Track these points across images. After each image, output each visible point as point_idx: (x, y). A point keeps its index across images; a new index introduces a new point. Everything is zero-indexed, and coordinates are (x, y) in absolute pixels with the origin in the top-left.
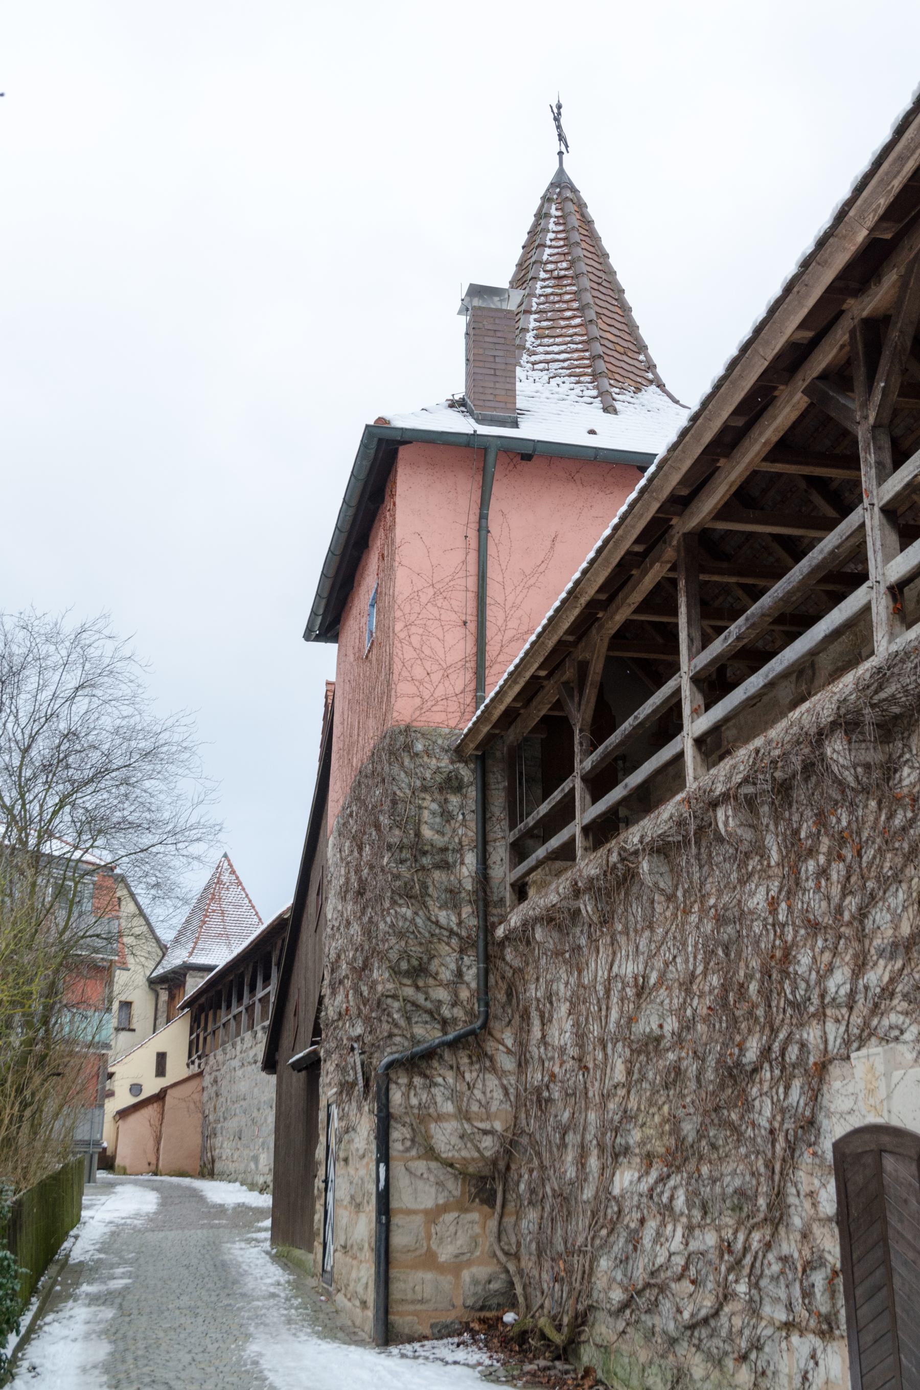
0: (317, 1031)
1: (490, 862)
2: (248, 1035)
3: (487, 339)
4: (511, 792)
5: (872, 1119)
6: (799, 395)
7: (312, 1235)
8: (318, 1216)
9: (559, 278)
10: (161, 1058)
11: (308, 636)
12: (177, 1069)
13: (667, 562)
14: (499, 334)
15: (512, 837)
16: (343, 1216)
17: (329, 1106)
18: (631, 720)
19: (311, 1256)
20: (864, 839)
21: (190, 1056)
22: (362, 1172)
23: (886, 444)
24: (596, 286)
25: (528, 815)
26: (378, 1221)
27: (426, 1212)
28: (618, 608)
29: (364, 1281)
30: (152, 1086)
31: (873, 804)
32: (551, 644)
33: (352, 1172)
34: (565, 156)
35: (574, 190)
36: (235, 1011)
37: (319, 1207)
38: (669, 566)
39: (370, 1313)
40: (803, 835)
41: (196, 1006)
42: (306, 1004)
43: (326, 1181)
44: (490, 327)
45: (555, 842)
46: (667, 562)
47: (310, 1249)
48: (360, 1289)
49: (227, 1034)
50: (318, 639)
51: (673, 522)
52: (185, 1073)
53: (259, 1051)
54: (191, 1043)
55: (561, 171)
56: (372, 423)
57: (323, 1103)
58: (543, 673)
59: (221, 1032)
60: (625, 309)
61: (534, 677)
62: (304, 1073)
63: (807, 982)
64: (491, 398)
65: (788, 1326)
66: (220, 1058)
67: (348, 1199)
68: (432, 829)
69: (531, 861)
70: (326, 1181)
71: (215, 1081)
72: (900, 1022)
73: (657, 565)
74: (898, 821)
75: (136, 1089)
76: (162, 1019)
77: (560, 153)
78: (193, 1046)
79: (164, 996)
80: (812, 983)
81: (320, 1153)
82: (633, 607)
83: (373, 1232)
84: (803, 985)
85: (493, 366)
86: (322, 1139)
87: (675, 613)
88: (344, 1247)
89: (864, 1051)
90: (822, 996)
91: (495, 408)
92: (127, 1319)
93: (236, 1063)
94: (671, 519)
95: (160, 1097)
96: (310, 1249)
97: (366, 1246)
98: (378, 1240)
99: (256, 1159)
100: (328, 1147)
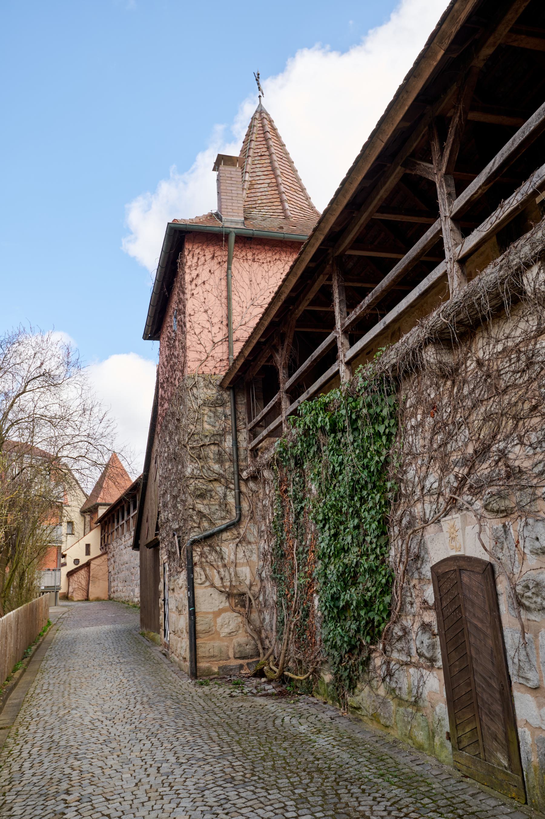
0: (157, 529)
1: (239, 439)
3: (228, 182)
5: (453, 553)
6: (399, 167)
7: (159, 626)
8: (162, 617)
9: (261, 156)
10: (88, 546)
12: (95, 551)
13: (327, 274)
14: (233, 179)
15: (249, 426)
16: (173, 616)
17: (164, 564)
18: (310, 357)
19: (159, 636)
20: (444, 403)
21: (101, 545)
22: (181, 595)
23: (452, 183)
27: (214, 613)
28: (301, 303)
29: (184, 648)
30: (84, 560)
31: (449, 383)
32: (266, 323)
33: (177, 595)
34: (262, 98)
35: (267, 114)
36: (121, 523)
38: (327, 276)
39: (188, 664)
40: (408, 406)
41: (103, 522)
42: (152, 516)
43: (164, 600)
44: (229, 176)
45: (272, 426)
46: (327, 274)
48: (183, 654)
49: (118, 534)
50: (150, 338)
51: (329, 251)
52: (100, 553)
54: (101, 539)
55: (260, 105)
56: (171, 222)
57: (161, 562)
59: (115, 533)
60: (295, 171)
61: (258, 343)
62: (152, 549)
63: (413, 483)
64: (231, 210)
66: (115, 545)
67: (175, 608)
68: (209, 424)
69: (260, 437)
70: (164, 600)
71: (113, 556)
72: (470, 499)
73: (321, 277)
74: (466, 391)
75: (76, 561)
76: (88, 529)
78: (103, 539)
79: (88, 518)
80: (416, 483)
81: (161, 587)
82: (308, 302)
83: (188, 624)
84: (411, 485)
85: (230, 195)
86: (162, 580)
87: (330, 301)
88: (174, 632)
89: (448, 518)
92: (67, 673)
93: (122, 547)
94: (328, 250)
95: (88, 565)
96: (159, 633)
97: (185, 631)
99: (133, 591)
100: (165, 583)
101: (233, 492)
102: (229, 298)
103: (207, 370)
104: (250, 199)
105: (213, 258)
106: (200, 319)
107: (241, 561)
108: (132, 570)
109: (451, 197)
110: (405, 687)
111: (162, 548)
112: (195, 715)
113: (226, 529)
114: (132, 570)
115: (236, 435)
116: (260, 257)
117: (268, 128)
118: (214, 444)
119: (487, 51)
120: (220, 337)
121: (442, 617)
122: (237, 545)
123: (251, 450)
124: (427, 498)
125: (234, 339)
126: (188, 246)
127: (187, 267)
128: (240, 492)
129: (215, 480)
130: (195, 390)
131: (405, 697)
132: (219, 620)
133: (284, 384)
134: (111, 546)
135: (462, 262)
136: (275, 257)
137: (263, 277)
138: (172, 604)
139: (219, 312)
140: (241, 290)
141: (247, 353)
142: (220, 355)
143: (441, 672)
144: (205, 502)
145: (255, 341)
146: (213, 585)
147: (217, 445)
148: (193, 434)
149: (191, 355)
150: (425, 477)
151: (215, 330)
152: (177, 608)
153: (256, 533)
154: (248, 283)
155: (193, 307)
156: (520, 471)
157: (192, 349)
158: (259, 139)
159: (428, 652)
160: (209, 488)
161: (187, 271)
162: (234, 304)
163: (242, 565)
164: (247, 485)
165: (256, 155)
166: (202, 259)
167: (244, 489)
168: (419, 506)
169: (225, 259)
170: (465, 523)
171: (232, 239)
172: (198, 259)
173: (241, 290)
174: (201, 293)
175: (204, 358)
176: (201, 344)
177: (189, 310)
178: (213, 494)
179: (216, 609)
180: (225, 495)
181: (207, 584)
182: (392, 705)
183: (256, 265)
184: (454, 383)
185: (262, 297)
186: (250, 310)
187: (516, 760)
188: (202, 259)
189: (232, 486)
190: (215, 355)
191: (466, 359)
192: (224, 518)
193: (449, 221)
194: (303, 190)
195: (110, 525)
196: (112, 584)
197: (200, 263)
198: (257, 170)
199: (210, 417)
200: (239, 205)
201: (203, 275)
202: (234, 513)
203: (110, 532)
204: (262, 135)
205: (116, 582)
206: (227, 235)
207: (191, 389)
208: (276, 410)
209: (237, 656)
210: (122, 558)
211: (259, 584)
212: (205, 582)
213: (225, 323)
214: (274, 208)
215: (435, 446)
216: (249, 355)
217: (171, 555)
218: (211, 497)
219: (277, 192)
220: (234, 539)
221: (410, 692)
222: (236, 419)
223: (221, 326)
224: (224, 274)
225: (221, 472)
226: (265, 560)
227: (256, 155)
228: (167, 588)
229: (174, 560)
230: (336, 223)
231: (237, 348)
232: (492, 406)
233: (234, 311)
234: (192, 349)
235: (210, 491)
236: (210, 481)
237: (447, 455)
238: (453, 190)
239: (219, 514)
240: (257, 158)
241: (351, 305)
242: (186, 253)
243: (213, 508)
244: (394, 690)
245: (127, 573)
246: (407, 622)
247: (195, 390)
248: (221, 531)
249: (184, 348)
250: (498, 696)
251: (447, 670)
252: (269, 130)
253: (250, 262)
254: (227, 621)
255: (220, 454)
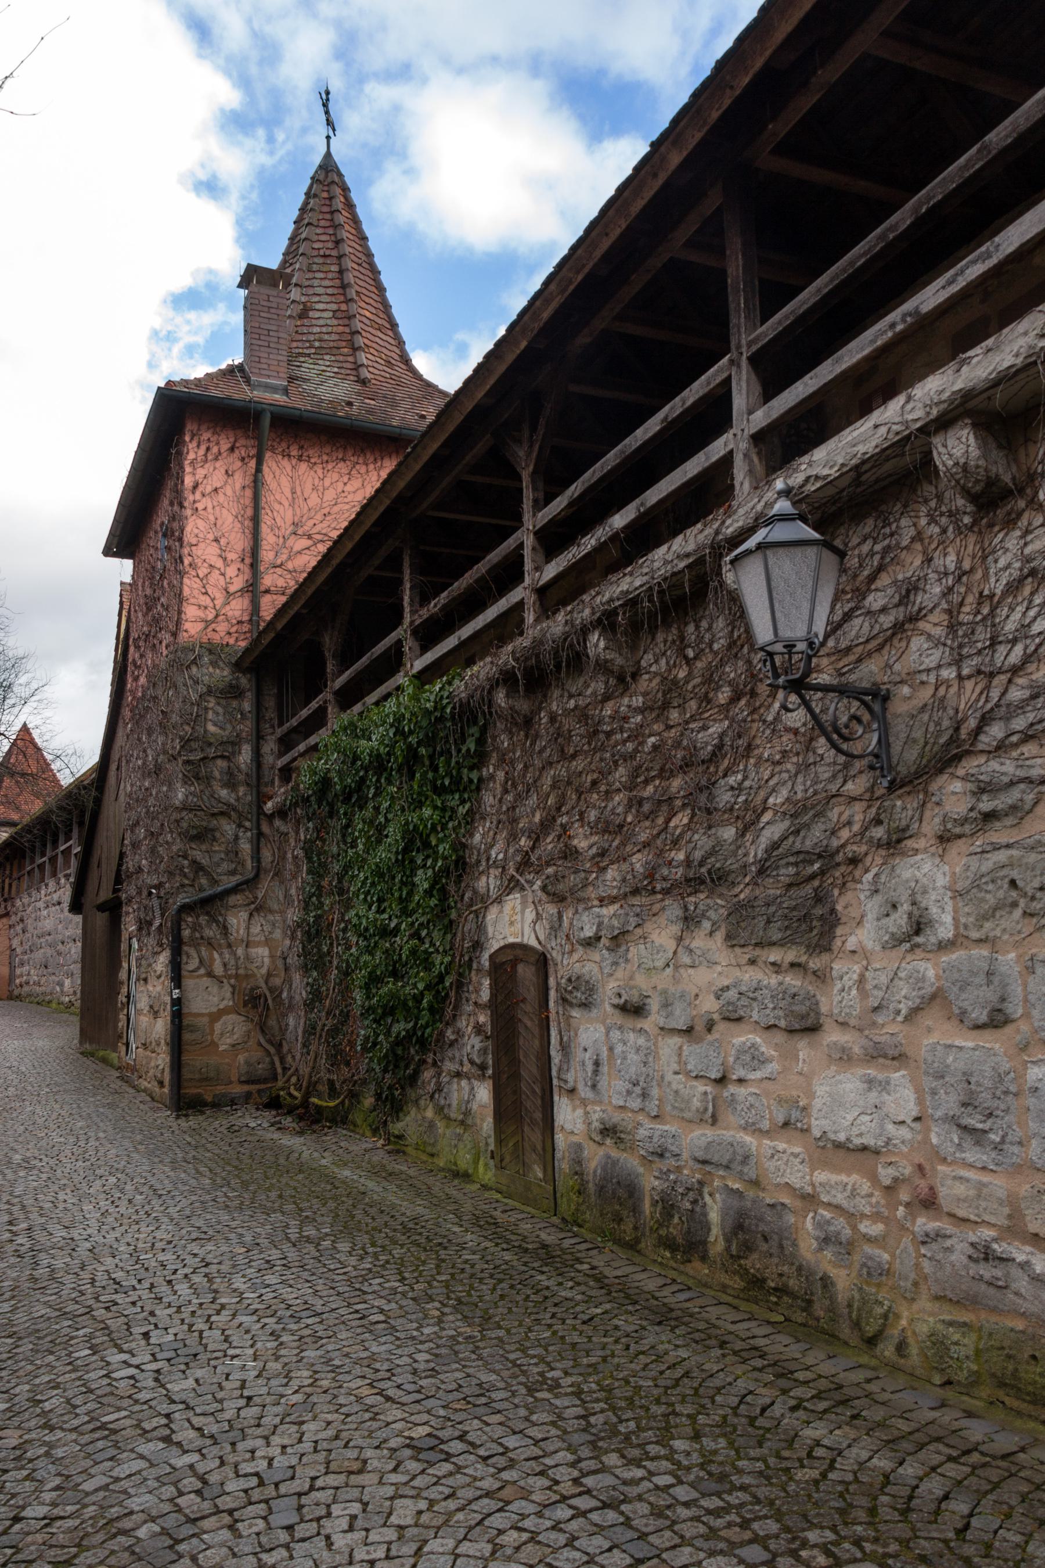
0: (118, 880)
2: (52, 883)
4: (279, 696)
9: (325, 256)
11: (107, 552)
15: (279, 732)
22: (159, 988)
24: (356, 267)
25: (294, 715)
26: (172, 1022)
27: (210, 1015)
33: (151, 988)
34: (332, 141)
35: (340, 175)
37: (122, 1017)
47: (115, 1049)
53: (65, 894)
55: (328, 155)
56: (162, 385)
57: (125, 936)
58: (304, 611)
60: (381, 289)
61: (297, 615)
62: (107, 913)
65: (458, 1075)
68: (215, 725)
69: (294, 753)
70: (128, 997)
71: (22, 920)
77: (328, 138)
81: (123, 975)
86: (125, 965)
88: (144, 1045)
90: (488, 859)
91: (269, 376)
98: (172, 1038)
101: (249, 834)
102: (256, 520)
103: (216, 638)
104: (300, 337)
105: (232, 449)
106: (206, 553)
107: (257, 939)
108: (60, 947)
109: (539, 505)
110: (455, 1103)
111: (127, 913)
112: (178, 1151)
113: (234, 890)
114: (60, 947)
115: (258, 743)
116: (311, 452)
117: (339, 203)
118: (222, 757)
119: (583, 339)
120: (238, 584)
121: (495, 1017)
122: (251, 915)
123: (280, 770)
124: (491, 871)
125: (262, 588)
126: (190, 426)
127: (187, 462)
128: (260, 834)
129: (222, 813)
130: (194, 669)
131: (453, 1115)
132: (218, 1026)
133: (333, 681)
134: (18, 903)
135: (542, 592)
136: (335, 455)
137: (315, 488)
138: (142, 1002)
139: (238, 541)
140: (276, 506)
141: (279, 626)
142: (237, 614)
143: (491, 1082)
144: (204, 847)
145: (292, 612)
146: (210, 974)
147: (227, 758)
148: (189, 740)
149: (191, 612)
150: (492, 846)
151: (231, 571)
152: (151, 1007)
153: (281, 897)
154: (289, 495)
155: (196, 531)
156: (577, 852)
157: (192, 601)
158: (322, 223)
159: (479, 1057)
160: (211, 826)
161: (188, 469)
162: (264, 529)
163: (258, 944)
164: (271, 824)
165: (315, 253)
166: (215, 450)
167: (265, 828)
168: (484, 879)
169: (253, 452)
170: (524, 903)
171: (267, 421)
172: (208, 449)
173: (276, 506)
174: (209, 509)
175: (210, 617)
176: (206, 593)
177: (189, 537)
178: (218, 835)
179: (214, 1010)
180: (237, 838)
181: (202, 971)
182: (440, 1125)
183: (303, 466)
184: (527, 736)
185: (312, 522)
186: (289, 543)
187: (550, 1169)
188: (215, 450)
189: (247, 824)
190: (230, 613)
191: (540, 709)
192: (233, 873)
193: (532, 536)
194: (394, 326)
195: (16, 863)
196: (18, 971)
197: (210, 457)
198: (316, 283)
199: (217, 714)
200: (280, 358)
201: (215, 478)
202: (249, 864)
203: (15, 875)
204: (328, 216)
205: (26, 968)
206: (258, 415)
207: (188, 667)
208: (318, 720)
209: (243, 1079)
210: (40, 924)
211: (283, 974)
212: (198, 968)
213: (248, 561)
214: (341, 358)
215: (504, 808)
216: (283, 629)
217: (144, 925)
218: (214, 839)
219: (347, 330)
220: (248, 905)
221: (459, 1109)
222: (259, 719)
223: (241, 566)
224: (249, 480)
225: (232, 801)
226: (293, 938)
227: (315, 253)
228: (134, 977)
229: (149, 934)
230: (408, 487)
231: (269, 607)
232: (561, 771)
233: (264, 542)
234: (192, 601)
235: (213, 830)
236: (213, 815)
237: (515, 821)
238: (541, 495)
239: (225, 866)
240: (316, 260)
241: (424, 597)
242: (187, 438)
243: (216, 858)
244: (442, 1108)
245: (49, 952)
246: (462, 1023)
247: (194, 669)
248: (228, 892)
249: (180, 598)
250: (539, 1102)
251: (496, 1079)
252: (340, 206)
253: (294, 461)
254: (230, 1028)
255: (230, 773)
